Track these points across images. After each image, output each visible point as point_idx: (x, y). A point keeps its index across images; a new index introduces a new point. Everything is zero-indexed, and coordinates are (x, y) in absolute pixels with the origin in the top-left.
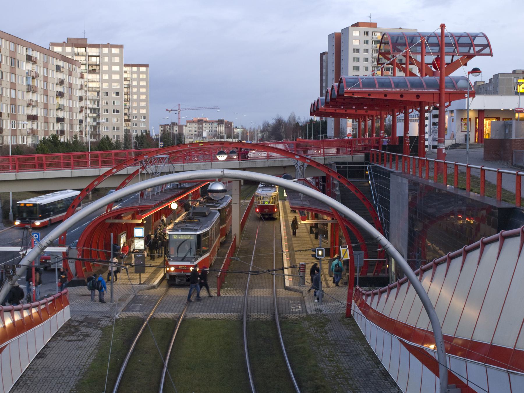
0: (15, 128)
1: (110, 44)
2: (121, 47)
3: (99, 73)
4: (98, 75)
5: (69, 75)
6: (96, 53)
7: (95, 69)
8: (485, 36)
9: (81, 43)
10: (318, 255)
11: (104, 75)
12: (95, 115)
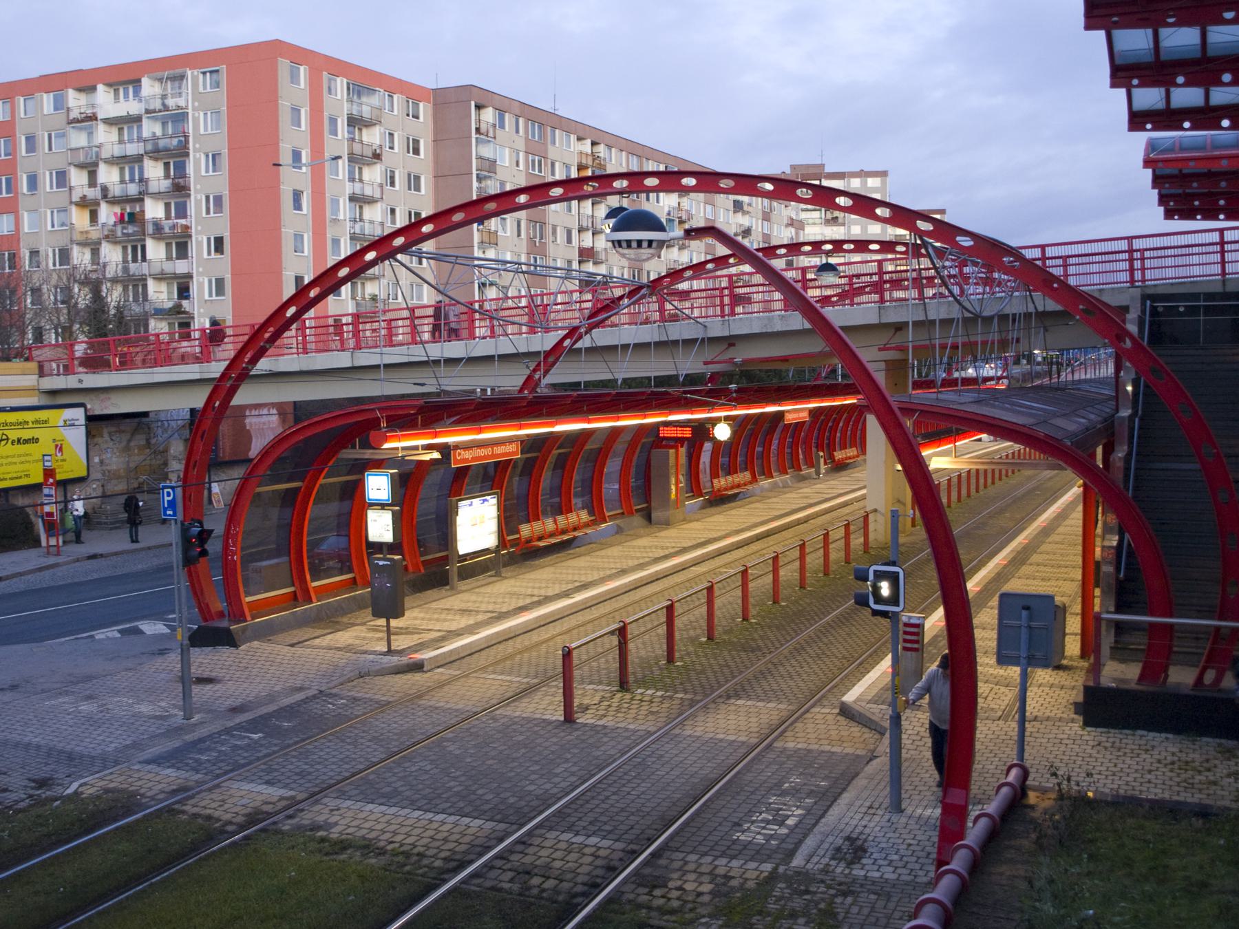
2: (883, 174)
3: (843, 224)
4: (842, 228)
7: (837, 218)
10: (879, 599)
11: (852, 227)
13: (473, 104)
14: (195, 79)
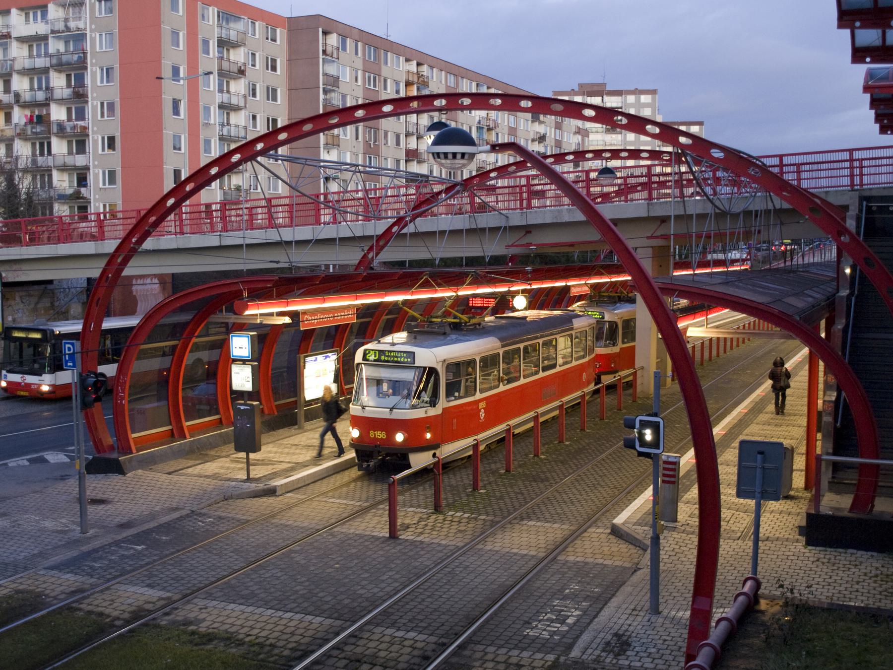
5: (555, 128)
6: (617, 102)
9: (599, 91)
10: (643, 443)
13: (320, 30)
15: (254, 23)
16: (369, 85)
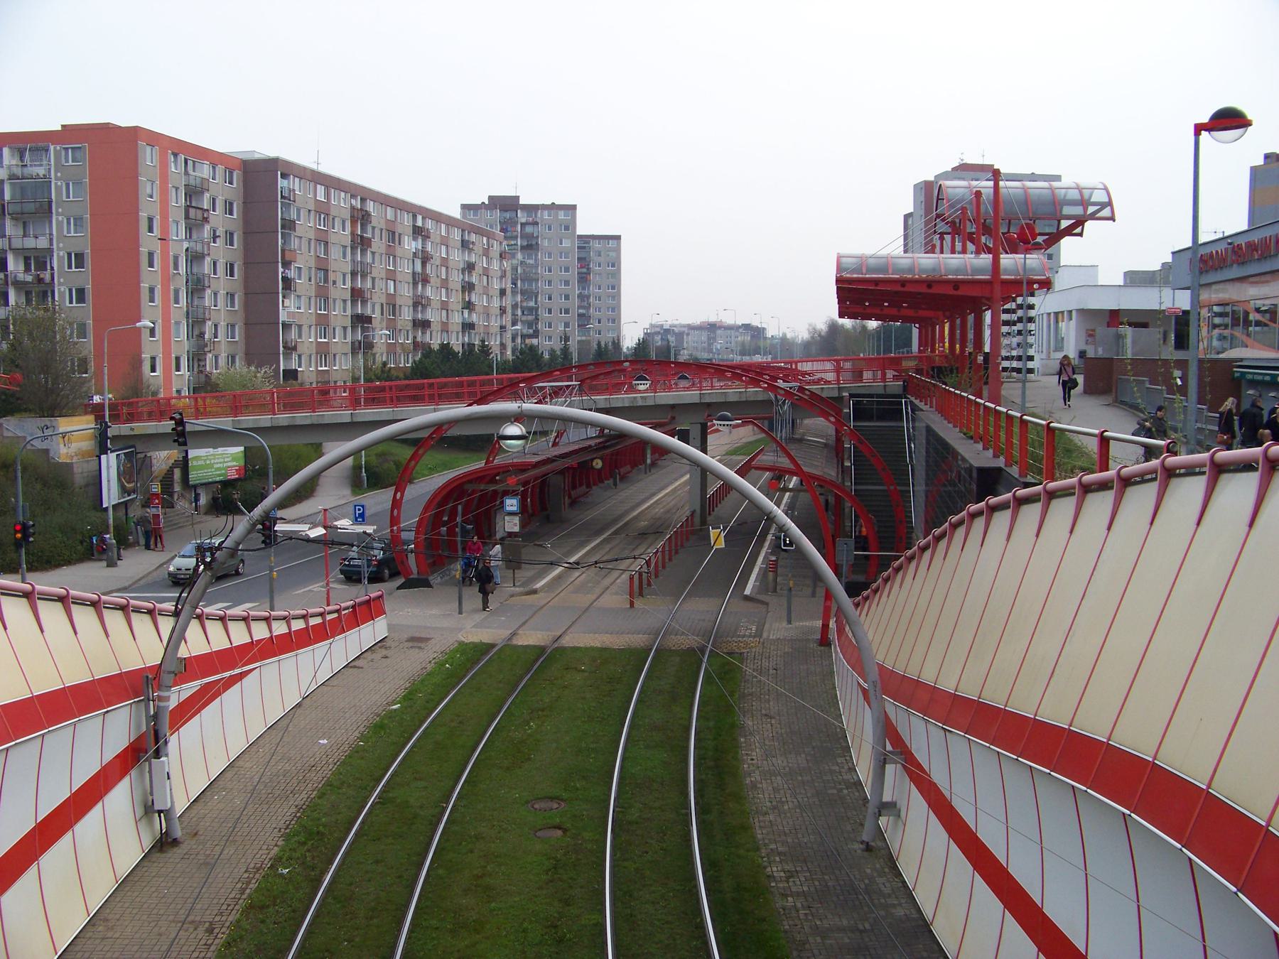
0: (326, 340)
1: (1036, 173)
8: (1106, 189)
12: (530, 318)
13: (279, 173)
14: (57, 154)
15: (232, 172)
16: (320, 225)
